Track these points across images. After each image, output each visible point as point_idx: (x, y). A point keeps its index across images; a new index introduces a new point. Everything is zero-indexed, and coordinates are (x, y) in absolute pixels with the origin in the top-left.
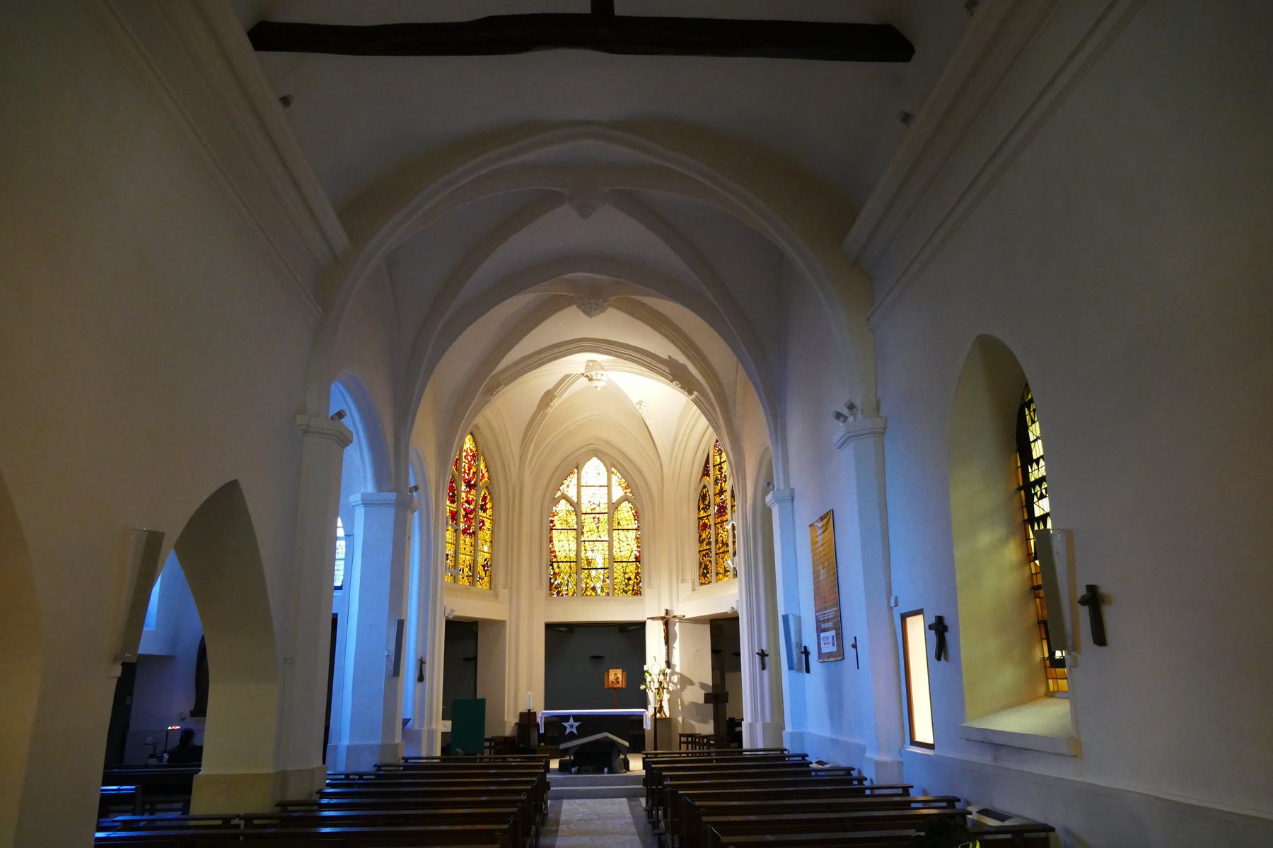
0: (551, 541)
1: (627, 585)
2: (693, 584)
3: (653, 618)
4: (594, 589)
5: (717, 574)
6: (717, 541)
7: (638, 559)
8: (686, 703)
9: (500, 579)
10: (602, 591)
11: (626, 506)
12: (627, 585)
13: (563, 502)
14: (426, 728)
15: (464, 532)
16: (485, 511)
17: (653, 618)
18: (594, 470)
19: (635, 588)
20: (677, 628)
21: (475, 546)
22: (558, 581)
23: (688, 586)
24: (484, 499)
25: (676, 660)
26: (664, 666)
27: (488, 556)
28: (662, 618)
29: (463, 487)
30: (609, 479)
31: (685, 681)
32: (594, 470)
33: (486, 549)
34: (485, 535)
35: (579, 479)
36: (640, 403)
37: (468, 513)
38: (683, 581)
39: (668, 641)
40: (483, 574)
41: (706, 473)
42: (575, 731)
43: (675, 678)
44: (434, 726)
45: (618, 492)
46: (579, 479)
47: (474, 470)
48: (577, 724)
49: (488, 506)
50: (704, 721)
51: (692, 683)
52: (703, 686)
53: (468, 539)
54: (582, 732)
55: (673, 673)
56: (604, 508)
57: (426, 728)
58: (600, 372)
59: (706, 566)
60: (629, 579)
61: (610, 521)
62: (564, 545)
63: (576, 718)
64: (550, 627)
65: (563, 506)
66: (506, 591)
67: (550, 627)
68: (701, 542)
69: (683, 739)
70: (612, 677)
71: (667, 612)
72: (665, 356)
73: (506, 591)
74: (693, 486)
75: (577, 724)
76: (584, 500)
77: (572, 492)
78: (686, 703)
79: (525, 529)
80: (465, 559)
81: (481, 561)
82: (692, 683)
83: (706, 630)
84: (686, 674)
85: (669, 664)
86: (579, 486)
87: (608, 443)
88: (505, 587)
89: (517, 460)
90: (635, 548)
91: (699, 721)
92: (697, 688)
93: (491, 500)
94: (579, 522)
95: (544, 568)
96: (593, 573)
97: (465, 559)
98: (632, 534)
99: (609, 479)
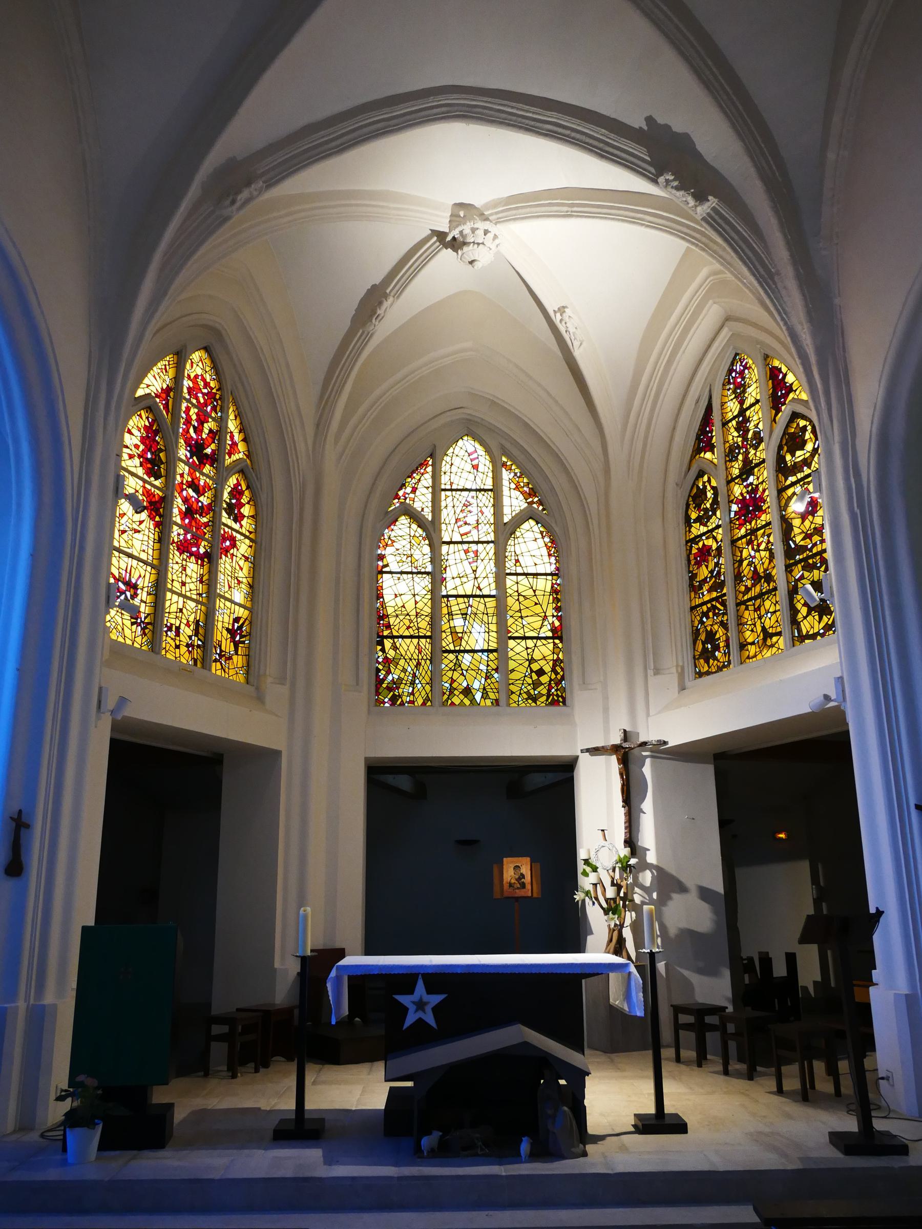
0: (380, 596)
1: (536, 684)
2: (681, 676)
3: (595, 751)
4: (467, 691)
5: (743, 646)
6: (738, 577)
7: (557, 634)
8: (672, 931)
9: (271, 668)
10: (485, 695)
11: (530, 531)
12: (536, 684)
13: (403, 520)
14: (21, 1005)
15: (183, 547)
16: (238, 518)
17: (595, 751)
18: (465, 463)
19: (553, 693)
20: (647, 770)
21: (210, 582)
22: (396, 674)
23: (670, 679)
24: (236, 492)
25: (648, 837)
26: (625, 852)
27: (242, 613)
28: (616, 749)
29: (183, 453)
30: (497, 479)
31: (668, 884)
32: (465, 463)
33: (239, 596)
34: (234, 569)
35: (436, 477)
36: (562, 310)
37: (189, 513)
38: (657, 672)
39: (630, 796)
40: (228, 647)
41: (703, 442)
42: (430, 1019)
43: (647, 878)
44: (49, 999)
45: (514, 503)
46: (436, 477)
47: (209, 425)
48: (435, 999)
49: (246, 510)
50: (709, 971)
51: (682, 889)
52: (705, 894)
53: (193, 568)
54: (452, 1024)
55: (644, 865)
56: (487, 532)
57: (21, 1005)
58: (482, 225)
59: (711, 636)
60: (540, 672)
61: (500, 559)
62: (402, 594)
63: (436, 980)
64: (379, 774)
65: (403, 527)
66: (285, 690)
67: (379, 774)
68: (694, 587)
69: (684, 1019)
70: (509, 874)
71: (626, 735)
72: (637, 121)
73: (285, 690)
74: (673, 477)
75: (435, 999)
76: (447, 515)
77: (422, 501)
78: (672, 931)
79: (326, 566)
80: (181, 609)
81: (223, 619)
82: (682, 889)
83: (706, 775)
84: (671, 869)
85: (631, 842)
86: (436, 490)
87: (494, 404)
88: (281, 680)
89: (310, 430)
90: (550, 611)
91: (700, 971)
92: (692, 898)
93: (253, 500)
94: (436, 558)
95: (364, 649)
96: (467, 659)
97: (181, 609)
98: (545, 585)
99: (497, 479)
